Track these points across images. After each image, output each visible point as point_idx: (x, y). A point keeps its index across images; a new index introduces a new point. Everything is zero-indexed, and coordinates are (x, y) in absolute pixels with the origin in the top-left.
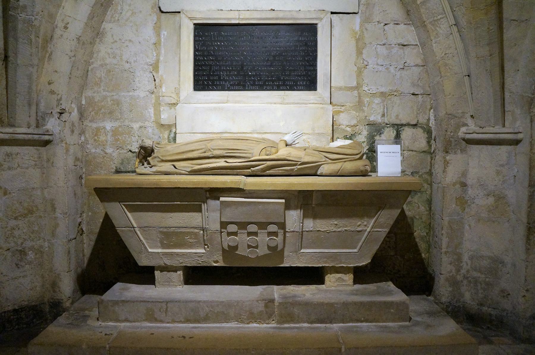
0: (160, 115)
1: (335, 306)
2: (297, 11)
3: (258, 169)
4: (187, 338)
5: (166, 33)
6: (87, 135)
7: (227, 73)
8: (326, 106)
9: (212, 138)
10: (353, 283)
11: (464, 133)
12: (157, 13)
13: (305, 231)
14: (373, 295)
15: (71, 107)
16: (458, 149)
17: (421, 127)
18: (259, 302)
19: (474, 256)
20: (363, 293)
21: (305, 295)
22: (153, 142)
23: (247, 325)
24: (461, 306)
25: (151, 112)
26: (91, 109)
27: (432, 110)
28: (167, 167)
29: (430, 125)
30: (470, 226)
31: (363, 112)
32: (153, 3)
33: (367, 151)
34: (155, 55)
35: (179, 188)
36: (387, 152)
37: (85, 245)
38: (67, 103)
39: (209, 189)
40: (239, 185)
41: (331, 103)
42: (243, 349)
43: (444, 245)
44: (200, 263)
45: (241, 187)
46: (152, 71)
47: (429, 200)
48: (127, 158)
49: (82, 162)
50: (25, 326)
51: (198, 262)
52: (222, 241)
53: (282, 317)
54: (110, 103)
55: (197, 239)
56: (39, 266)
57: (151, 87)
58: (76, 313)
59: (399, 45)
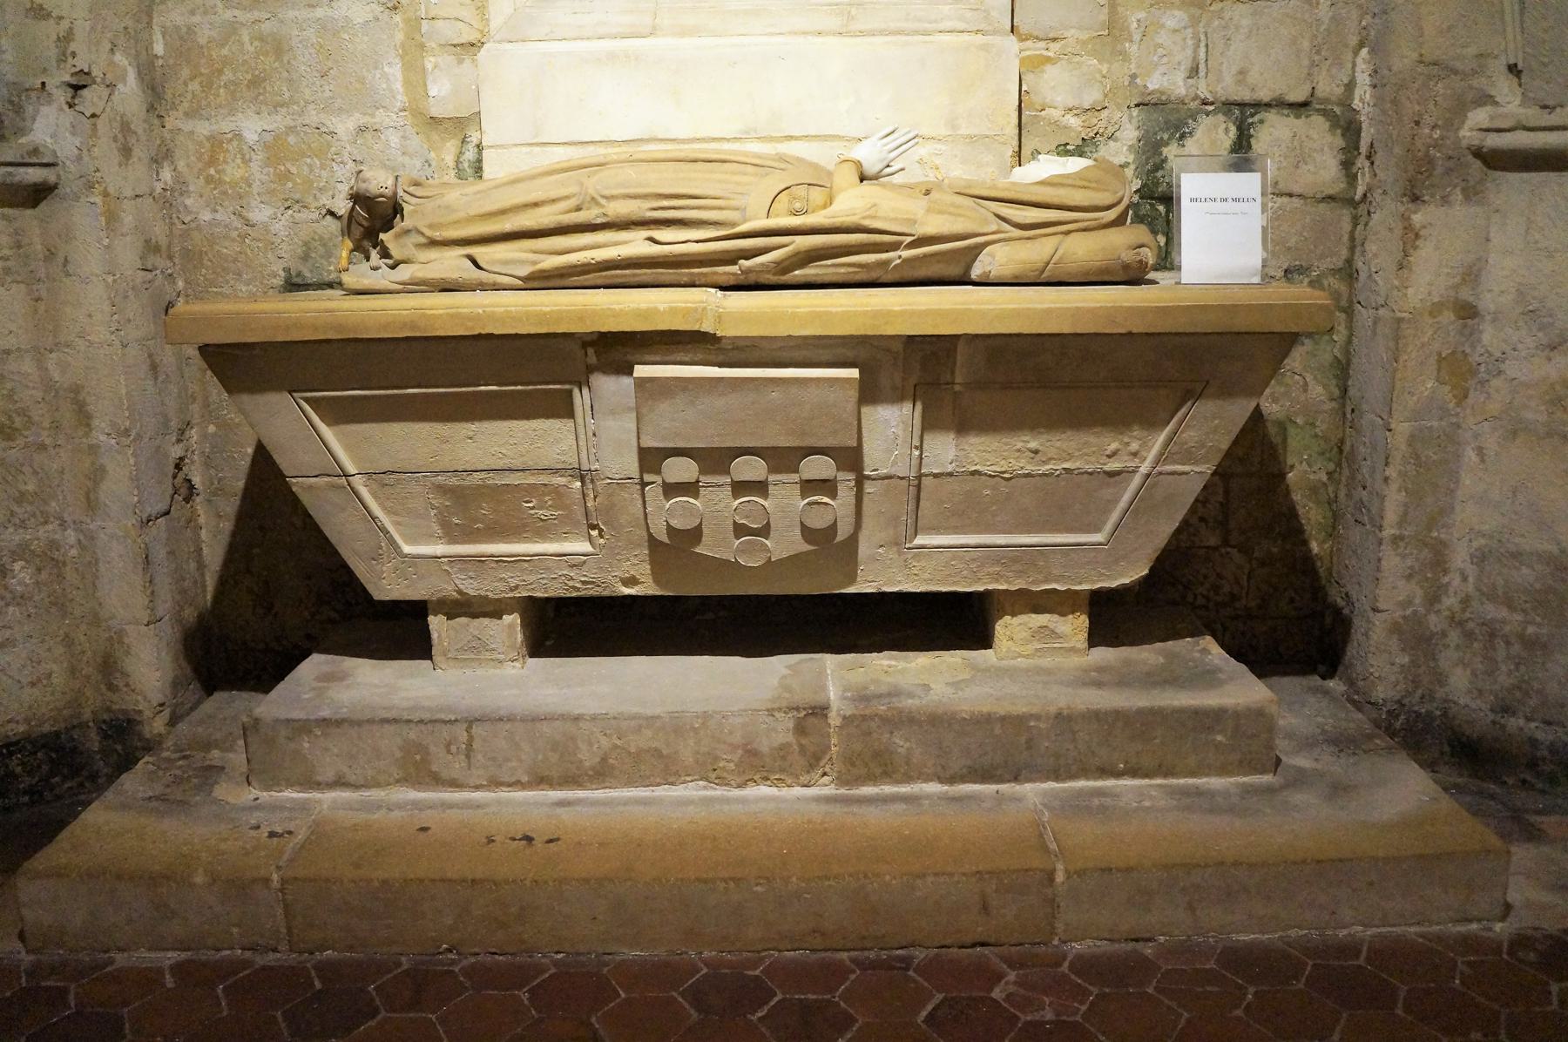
0: (425, 85)
1: (1032, 724)
3: (762, 264)
4: (538, 843)
6: (181, 165)
8: (996, 40)
9: (602, 160)
10: (1086, 645)
11: (1480, 130)
13: (926, 476)
14: (1155, 685)
15: (111, 63)
16: (1455, 187)
17: (1325, 113)
18: (776, 714)
19: (1490, 552)
20: (1122, 678)
21: (927, 687)
22: (397, 177)
24: (1438, 713)
25: (393, 75)
26: (185, 72)
27: (1364, 51)
28: (450, 263)
29: (1356, 104)
30: (1480, 451)
33: (1136, 198)
35: (490, 336)
36: (1212, 197)
37: (204, 531)
38: (94, 49)
39: (595, 337)
40: (700, 320)
41: (1012, 31)
42: (725, 880)
43: (1391, 515)
44: (578, 585)
45: (707, 327)
47: (1339, 361)
49: (170, 258)
50: (26, 799)
51: (571, 583)
53: (853, 764)
54: (252, 49)
56: (53, 610)
58: (180, 759)
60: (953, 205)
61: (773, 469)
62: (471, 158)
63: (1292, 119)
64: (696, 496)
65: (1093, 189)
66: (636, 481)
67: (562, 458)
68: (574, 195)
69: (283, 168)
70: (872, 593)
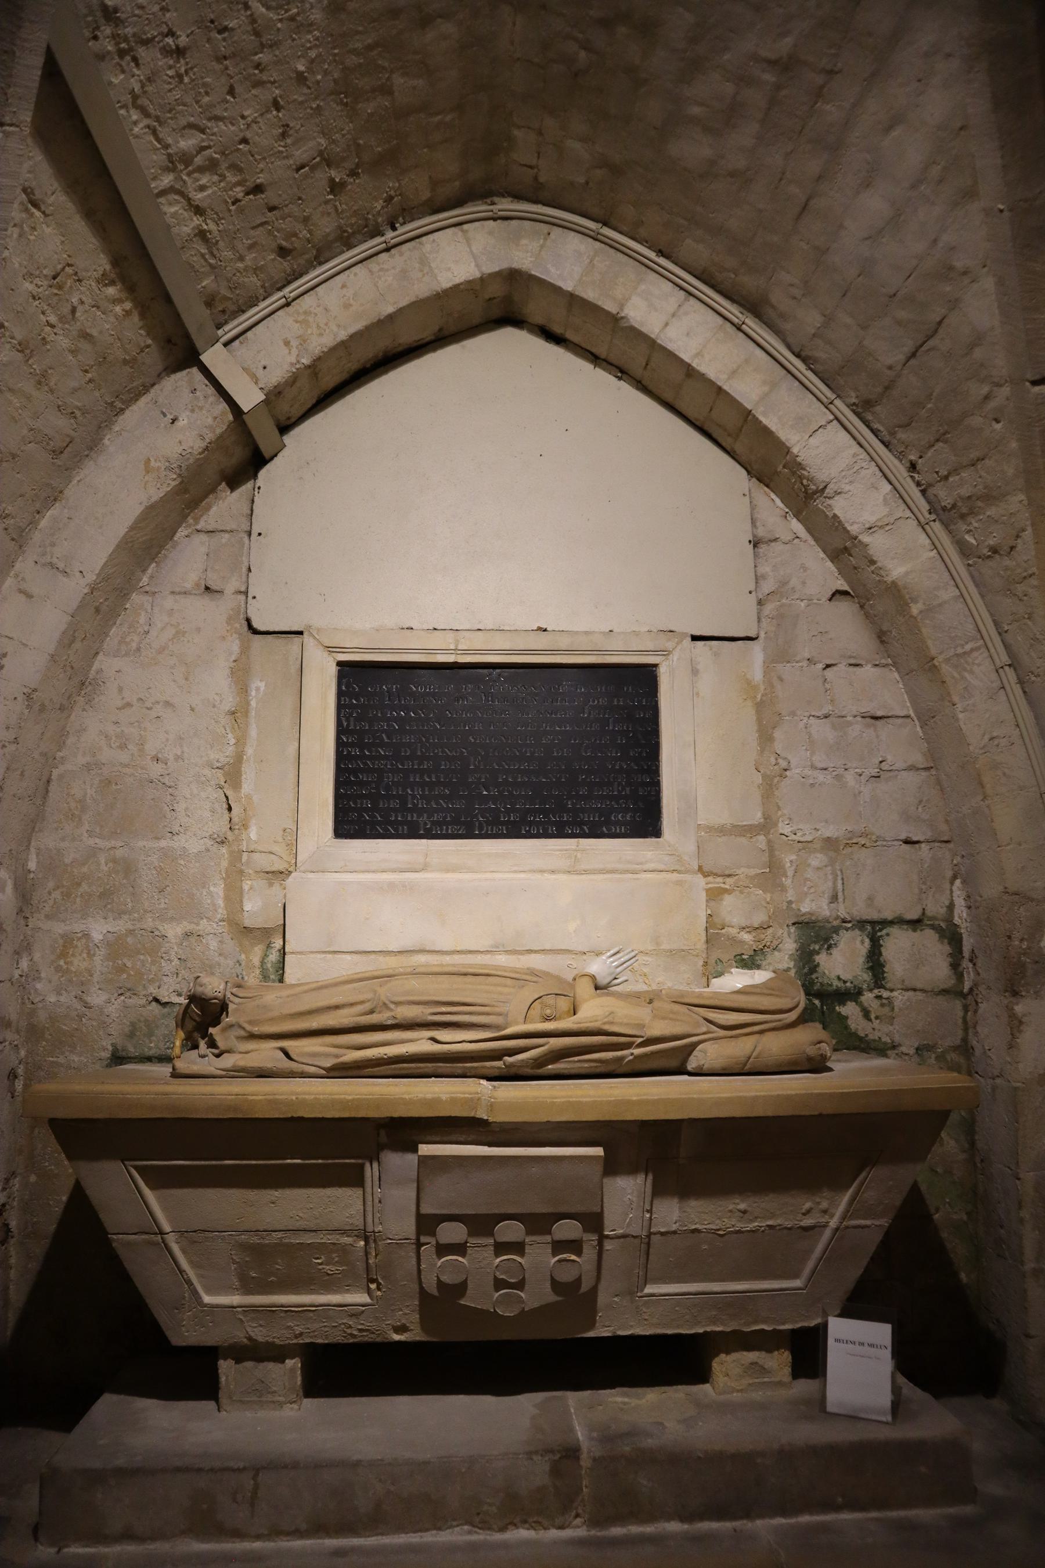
0: (242, 901)
2: (604, 633)
3: (523, 1061)
5: (262, 685)
6: (37, 956)
7: (423, 791)
8: (687, 877)
12: (240, 634)
17: (933, 927)
23: (498, 1537)
25: (217, 893)
26: (51, 884)
27: (958, 882)
28: (266, 1054)
29: (957, 920)
31: (782, 891)
32: (232, 610)
34: (233, 741)
44: (355, 1333)
46: (223, 784)
48: (148, 1021)
49: (18, 1032)
51: (349, 1331)
52: (419, 1271)
54: (106, 869)
55: (347, 1265)
57: (220, 825)
59: (863, 717)
60: (672, 1012)
61: (529, 1232)
62: (274, 960)
63: (910, 932)
64: (463, 1255)
65: (777, 996)
66: (412, 1241)
67: (351, 1221)
68: (369, 1001)
69: (120, 962)
70: (608, 1337)
